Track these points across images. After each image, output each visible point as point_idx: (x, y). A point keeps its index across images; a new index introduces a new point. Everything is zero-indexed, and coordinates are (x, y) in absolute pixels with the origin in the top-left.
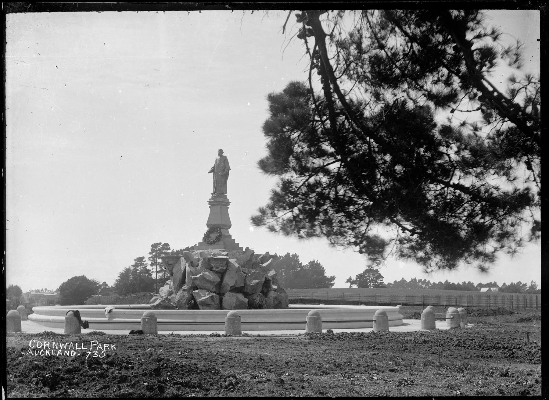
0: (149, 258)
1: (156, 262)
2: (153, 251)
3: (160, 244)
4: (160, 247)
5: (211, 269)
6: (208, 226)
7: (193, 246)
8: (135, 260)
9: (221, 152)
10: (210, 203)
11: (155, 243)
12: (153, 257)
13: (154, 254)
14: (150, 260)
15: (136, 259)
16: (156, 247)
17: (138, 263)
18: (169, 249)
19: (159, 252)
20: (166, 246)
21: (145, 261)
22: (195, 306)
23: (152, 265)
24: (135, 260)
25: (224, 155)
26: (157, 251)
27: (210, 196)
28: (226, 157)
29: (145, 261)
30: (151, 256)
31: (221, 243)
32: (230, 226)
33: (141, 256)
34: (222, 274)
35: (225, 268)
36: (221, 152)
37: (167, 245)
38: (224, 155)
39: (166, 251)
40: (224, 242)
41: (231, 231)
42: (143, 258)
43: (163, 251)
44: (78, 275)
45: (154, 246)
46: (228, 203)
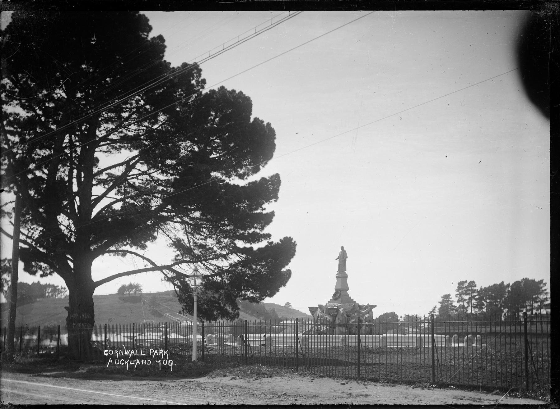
0: (456, 295)
1: (463, 299)
2: (459, 288)
3: (466, 282)
4: (466, 284)
5: (329, 314)
6: (335, 289)
7: (537, 280)
8: (442, 297)
9: (342, 248)
10: (336, 277)
11: (461, 281)
12: (460, 294)
13: (460, 291)
14: (457, 297)
15: (442, 296)
16: (463, 285)
17: (445, 299)
18: (475, 286)
19: (465, 289)
20: (472, 284)
21: (451, 298)
22: (320, 334)
23: (459, 301)
24: (442, 297)
25: (344, 249)
26: (463, 288)
27: (337, 273)
28: (345, 250)
29: (451, 298)
30: (458, 293)
31: (340, 299)
32: (348, 289)
33: (447, 294)
34: (335, 317)
35: (336, 313)
36: (342, 248)
37: (473, 282)
38: (344, 249)
39: (472, 288)
40: (342, 299)
41: (348, 292)
42: (449, 295)
43: (470, 288)
44: (388, 312)
45: (461, 283)
46: (347, 276)
